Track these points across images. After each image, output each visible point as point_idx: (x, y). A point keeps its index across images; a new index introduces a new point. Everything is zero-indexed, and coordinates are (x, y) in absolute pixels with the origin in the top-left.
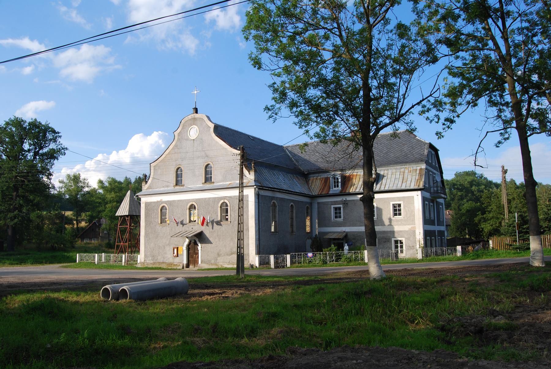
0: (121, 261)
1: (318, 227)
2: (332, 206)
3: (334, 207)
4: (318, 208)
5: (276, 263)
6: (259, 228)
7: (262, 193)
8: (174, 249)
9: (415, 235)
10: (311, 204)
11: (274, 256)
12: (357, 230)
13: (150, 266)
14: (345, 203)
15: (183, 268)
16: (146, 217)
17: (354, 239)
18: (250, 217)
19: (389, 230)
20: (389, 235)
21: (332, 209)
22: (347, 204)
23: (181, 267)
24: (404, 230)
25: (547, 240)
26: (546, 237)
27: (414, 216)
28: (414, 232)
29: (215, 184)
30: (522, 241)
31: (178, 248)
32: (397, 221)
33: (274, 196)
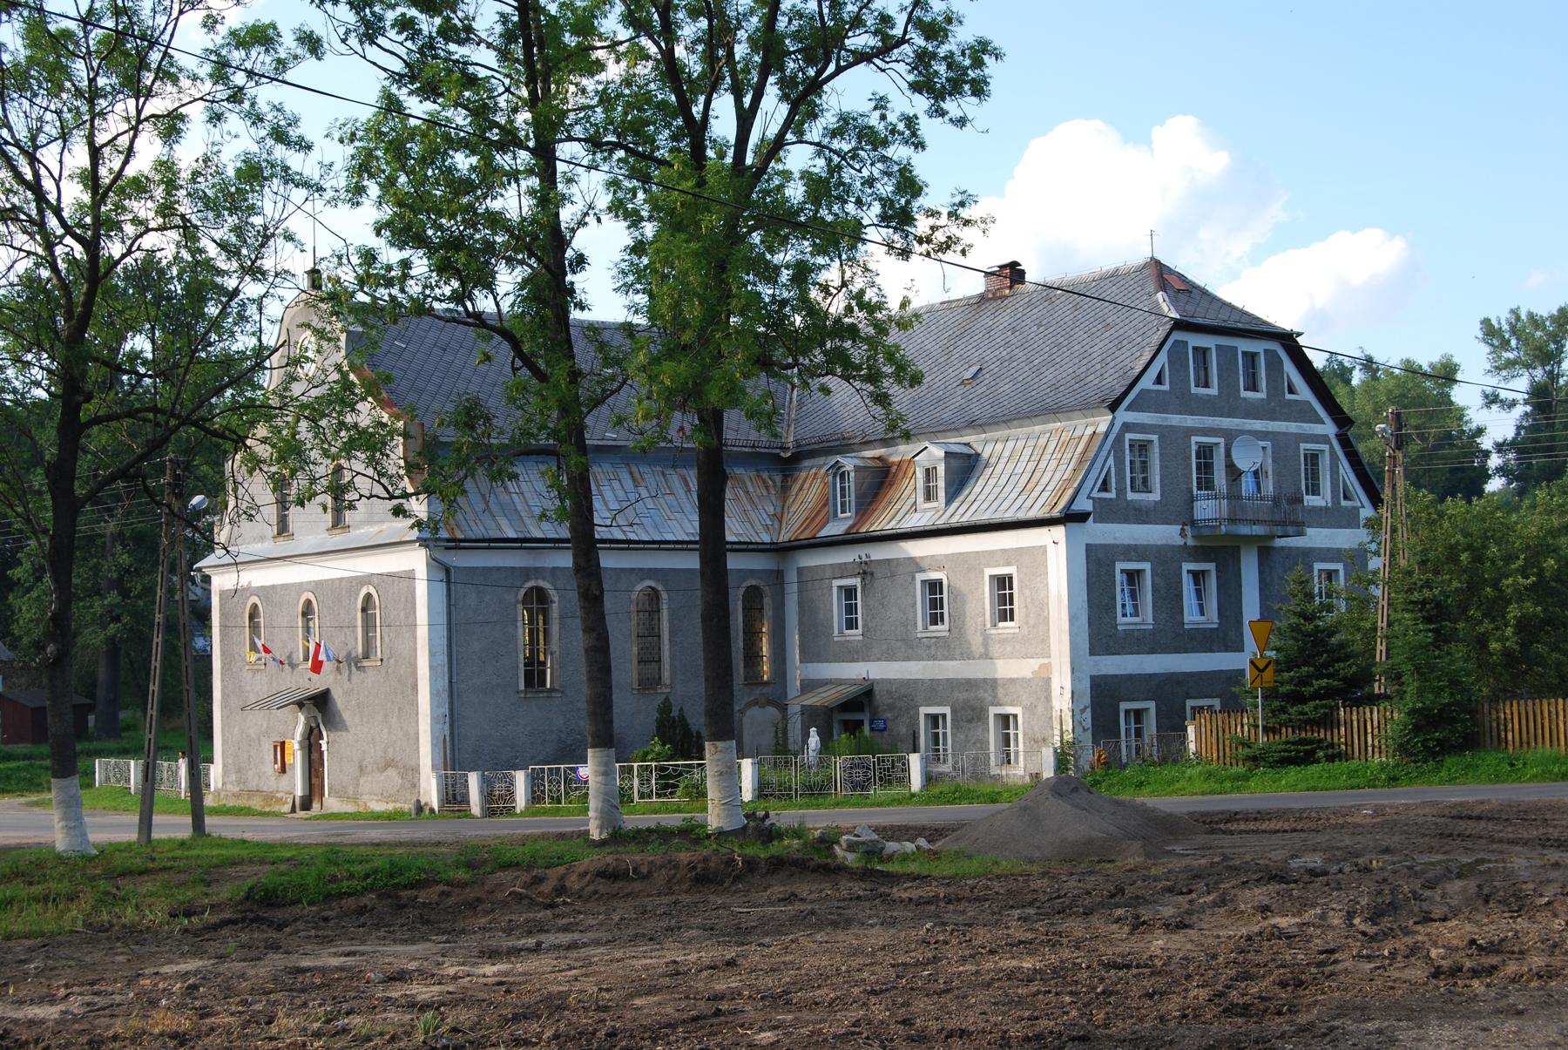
0: (128, 781)
1: (801, 662)
2: (837, 583)
3: (840, 588)
4: (800, 592)
5: (488, 796)
6: (450, 682)
7: (459, 560)
8: (275, 747)
9: (1048, 699)
10: (778, 577)
11: (483, 775)
12: (898, 676)
13: (231, 803)
14: (866, 571)
15: (293, 810)
16: (222, 641)
17: (891, 707)
18: (419, 646)
19: (981, 676)
20: (981, 694)
21: (835, 590)
22: (872, 574)
23: (287, 808)
24: (1020, 676)
25: (1369, 730)
26: (1368, 714)
27: (1046, 621)
28: (1047, 682)
29: (354, 533)
30: (1290, 730)
31: (283, 744)
32: (1004, 641)
33: (538, 564)
